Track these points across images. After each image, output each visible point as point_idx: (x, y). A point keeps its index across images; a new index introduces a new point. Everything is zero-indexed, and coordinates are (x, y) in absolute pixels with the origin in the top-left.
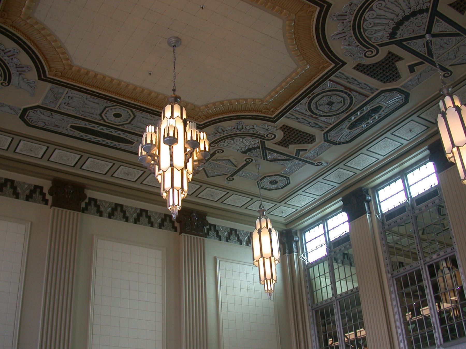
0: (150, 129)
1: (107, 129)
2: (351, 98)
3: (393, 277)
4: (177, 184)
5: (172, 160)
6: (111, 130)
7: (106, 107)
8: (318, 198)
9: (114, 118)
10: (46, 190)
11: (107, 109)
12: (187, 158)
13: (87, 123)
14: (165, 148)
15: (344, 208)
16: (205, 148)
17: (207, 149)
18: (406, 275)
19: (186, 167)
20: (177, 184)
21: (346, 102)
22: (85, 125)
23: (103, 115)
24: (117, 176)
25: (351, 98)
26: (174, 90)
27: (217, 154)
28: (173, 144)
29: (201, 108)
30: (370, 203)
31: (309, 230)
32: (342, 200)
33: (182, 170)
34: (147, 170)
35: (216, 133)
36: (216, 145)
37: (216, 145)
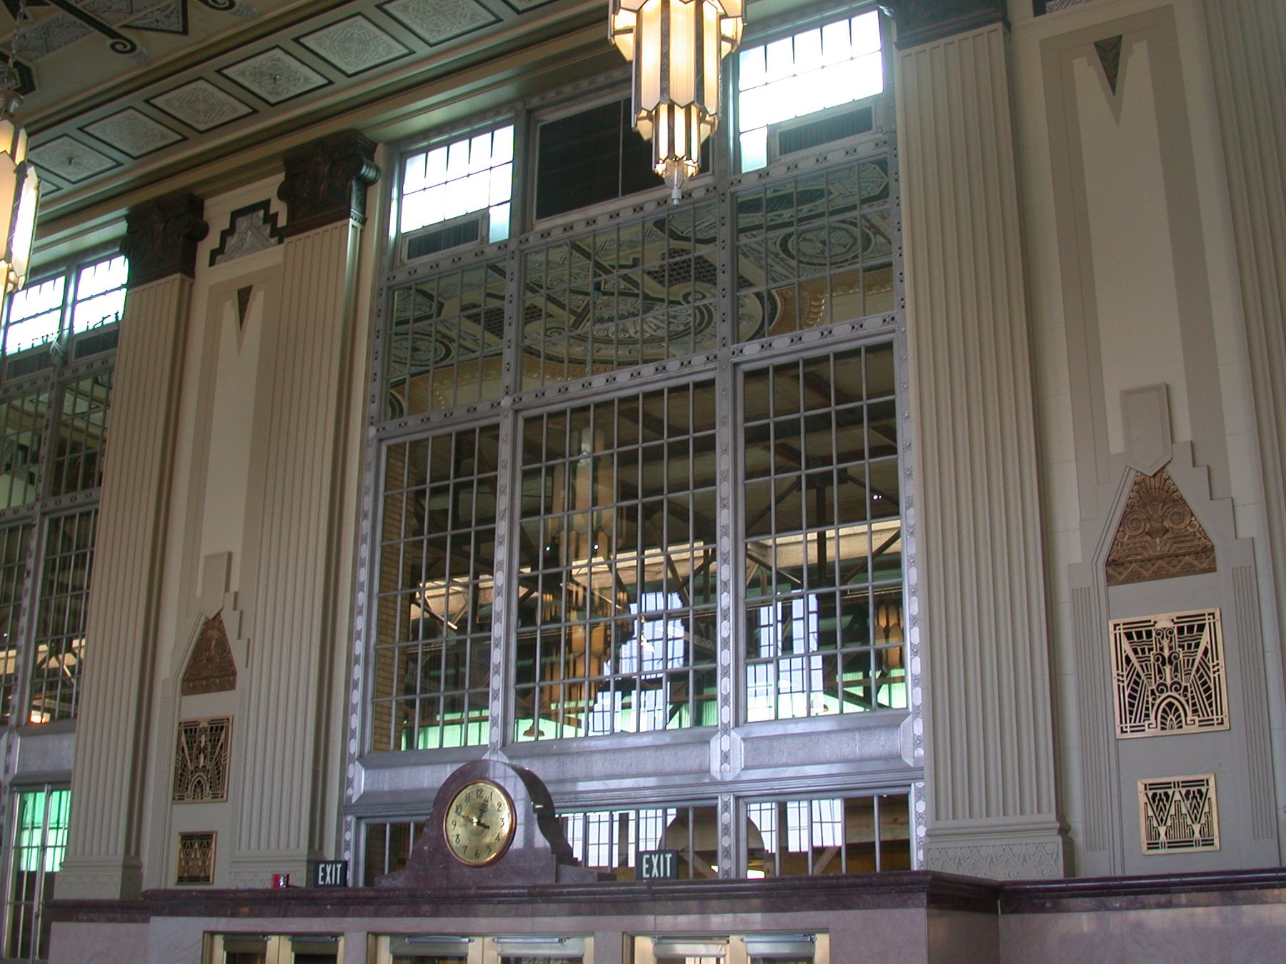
3: (381, 440)
8: (67, 187)
15: (126, 246)
18: (450, 435)
30: (370, 190)
31: (95, 263)
32: (127, 218)
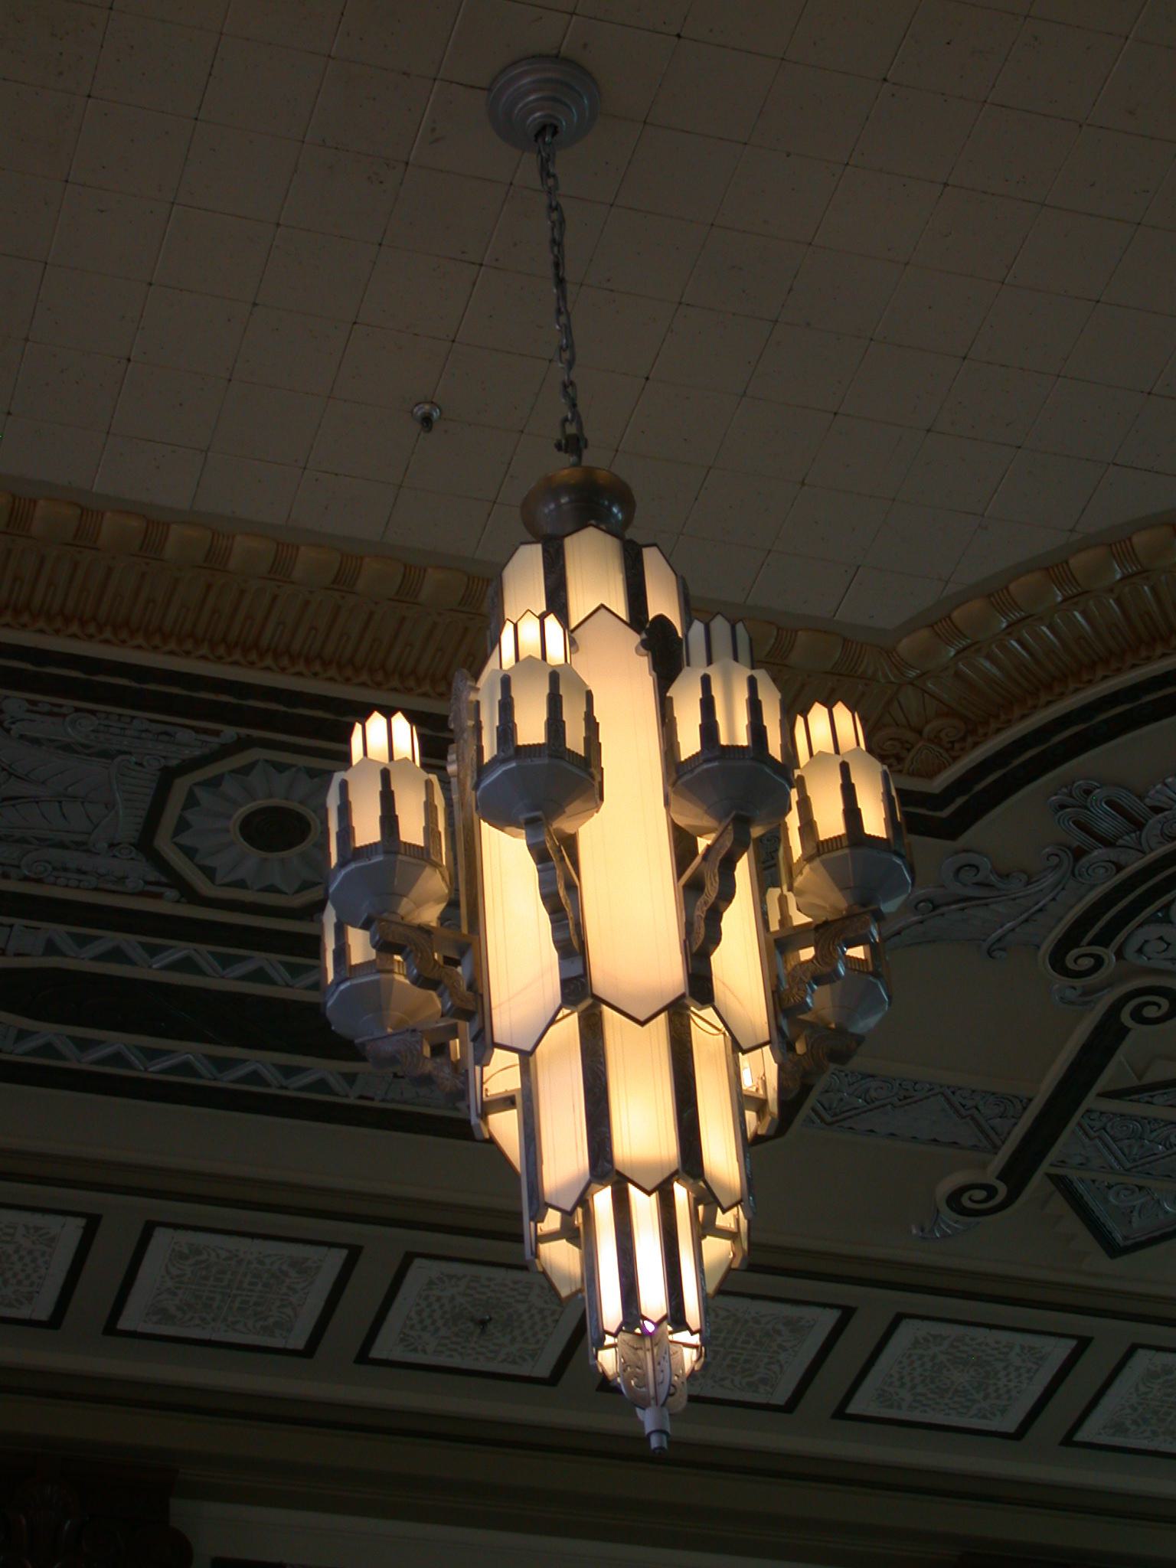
1: (226, 961)
5: (571, 942)
6: (260, 959)
7: (167, 777)
9: (255, 855)
11: (181, 787)
12: (700, 912)
13: (58, 932)
16: (852, 814)
17: (874, 823)
19: (700, 984)
22: (51, 948)
23: (163, 843)
24: (398, 1354)
26: (573, 445)
27: (1137, 1031)
28: (556, 808)
29: (904, 646)
33: (677, 1014)
35: (1079, 854)
36: (1109, 955)
37: (1109, 955)
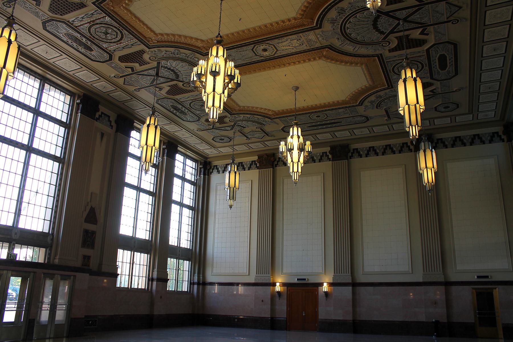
0: (202, 62)
2: (122, 35)
4: (217, 104)
10: (500, 133)
14: (210, 78)
19: (223, 93)
20: (217, 104)
21: (118, 37)
25: (122, 35)
34: (196, 90)
